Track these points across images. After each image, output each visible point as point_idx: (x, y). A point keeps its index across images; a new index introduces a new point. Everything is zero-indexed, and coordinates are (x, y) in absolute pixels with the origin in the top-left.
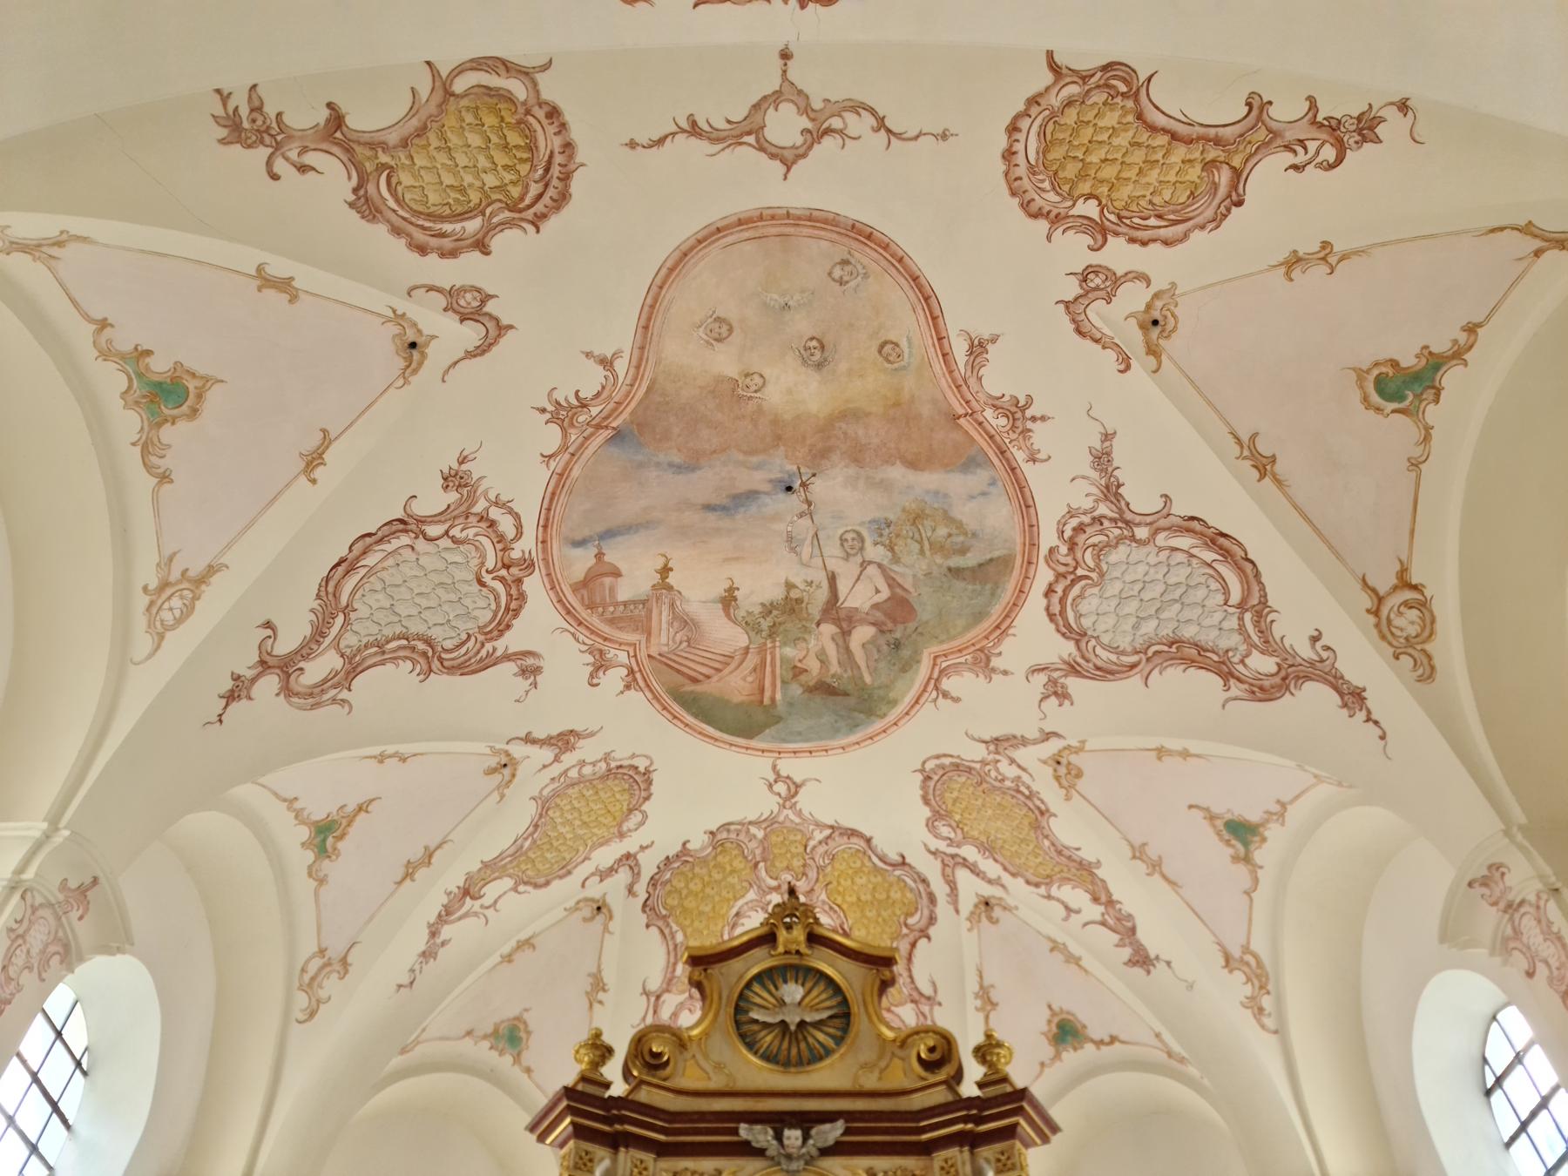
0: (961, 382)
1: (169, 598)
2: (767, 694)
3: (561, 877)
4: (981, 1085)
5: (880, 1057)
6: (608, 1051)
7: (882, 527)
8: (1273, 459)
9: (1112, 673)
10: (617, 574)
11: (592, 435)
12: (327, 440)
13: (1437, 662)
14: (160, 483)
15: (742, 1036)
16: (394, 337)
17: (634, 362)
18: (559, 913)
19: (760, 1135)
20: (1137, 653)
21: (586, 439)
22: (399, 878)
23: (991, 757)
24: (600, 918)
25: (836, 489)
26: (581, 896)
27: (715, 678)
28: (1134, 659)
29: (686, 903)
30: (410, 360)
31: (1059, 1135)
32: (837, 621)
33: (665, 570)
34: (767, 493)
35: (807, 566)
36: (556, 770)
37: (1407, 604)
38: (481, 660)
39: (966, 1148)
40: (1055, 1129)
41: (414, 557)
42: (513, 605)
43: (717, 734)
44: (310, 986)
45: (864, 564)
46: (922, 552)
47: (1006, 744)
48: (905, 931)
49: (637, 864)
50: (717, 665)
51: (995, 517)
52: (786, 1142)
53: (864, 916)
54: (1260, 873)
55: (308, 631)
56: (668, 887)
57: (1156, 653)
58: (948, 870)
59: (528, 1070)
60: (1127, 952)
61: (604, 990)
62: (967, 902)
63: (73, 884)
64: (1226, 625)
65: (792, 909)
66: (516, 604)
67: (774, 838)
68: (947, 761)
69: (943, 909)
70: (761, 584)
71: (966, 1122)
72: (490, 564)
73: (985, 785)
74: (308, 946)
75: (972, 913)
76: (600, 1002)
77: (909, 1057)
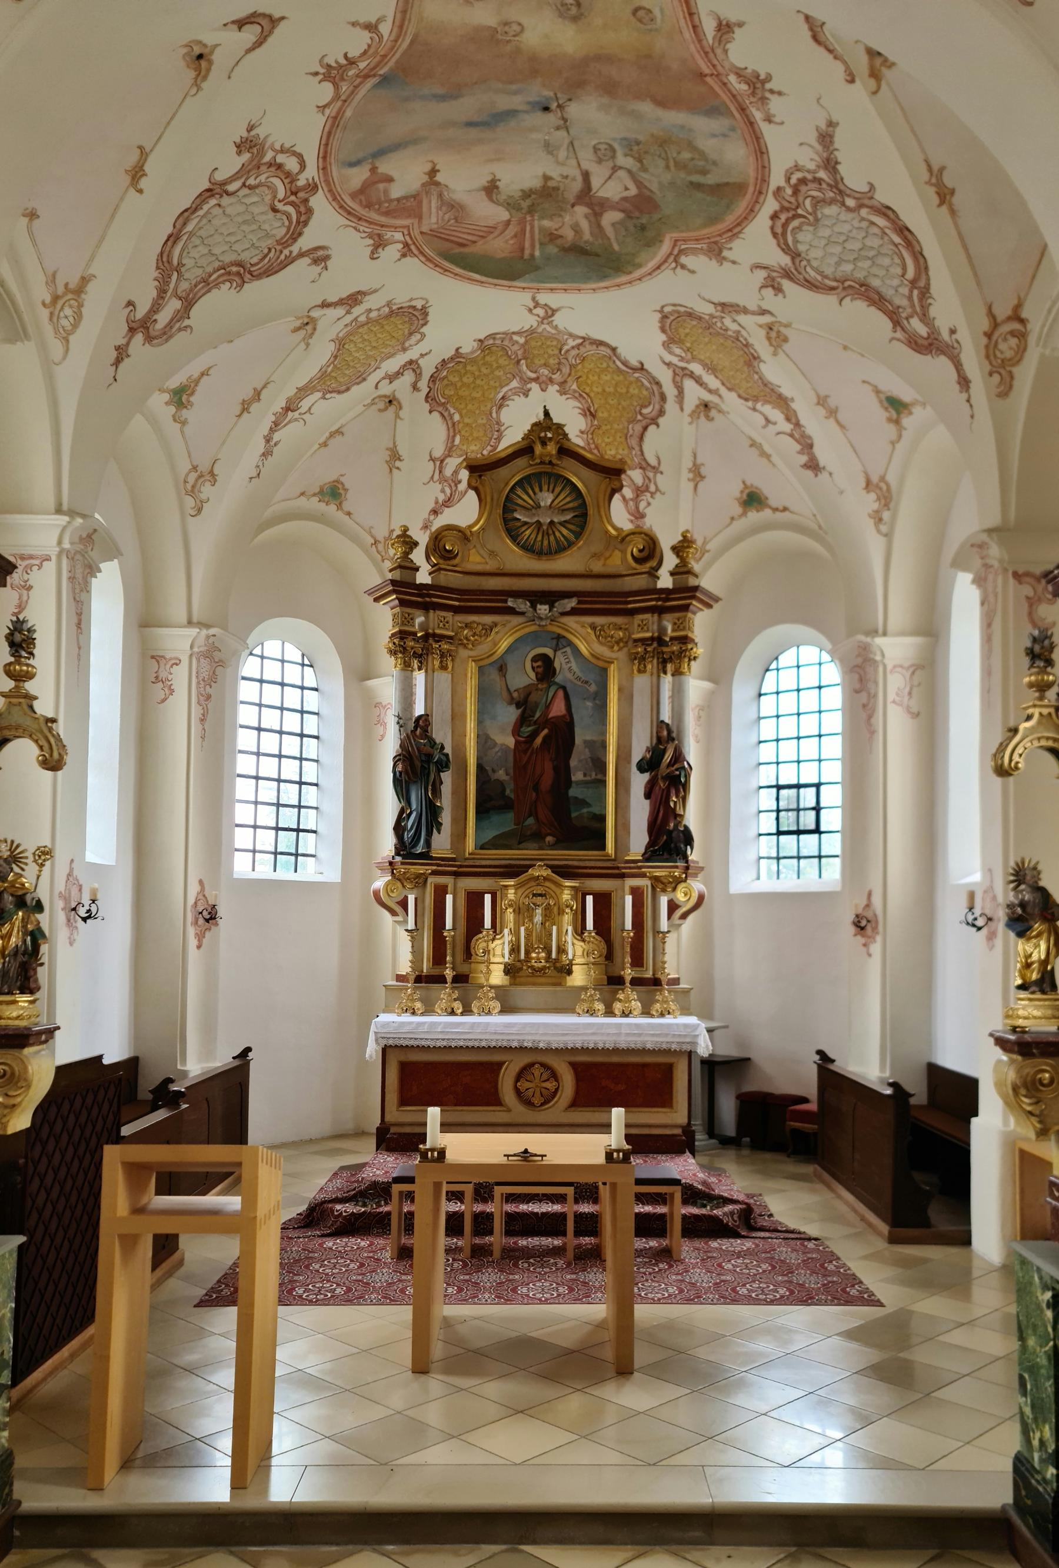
0: (708, 49)
1: (62, 309)
2: (527, 252)
3: (358, 384)
4: (672, 574)
7: (631, 146)
8: (952, 192)
9: (817, 287)
10: (390, 180)
11: (360, 83)
12: (144, 154)
13: (1015, 383)
14: (31, 220)
16: (184, 56)
17: (397, 23)
18: (360, 408)
19: (522, 605)
20: (836, 280)
21: (356, 87)
22: (238, 413)
23: (718, 314)
24: (392, 409)
25: (588, 112)
27: (481, 243)
28: (834, 284)
29: (461, 393)
30: (198, 70)
32: (590, 205)
33: (433, 172)
34: (526, 112)
35: (563, 164)
36: (349, 318)
37: (1013, 333)
38: (282, 262)
39: (656, 615)
40: (717, 600)
41: (220, 211)
42: (303, 218)
43: (484, 279)
44: (193, 492)
45: (615, 169)
46: (667, 167)
47: (731, 309)
48: (639, 417)
49: (419, 367)
50: (481, 234)
51: (734, 155)
54: (904, 433)
55: (154, 294)
56: (445, 382)
57: (850, 287)
58: (678, 379)
60: (804, 459)
63: (84, 536)
64: (901, 290)
66: (305, 215)
67: (533, 343)
68: (682, 309)
69: (671, 406)
70: (521, 174)
72: (281, 194)
73: (711, 330)
74: (184, 466)
75: (694, 412)
76: (398, 468)
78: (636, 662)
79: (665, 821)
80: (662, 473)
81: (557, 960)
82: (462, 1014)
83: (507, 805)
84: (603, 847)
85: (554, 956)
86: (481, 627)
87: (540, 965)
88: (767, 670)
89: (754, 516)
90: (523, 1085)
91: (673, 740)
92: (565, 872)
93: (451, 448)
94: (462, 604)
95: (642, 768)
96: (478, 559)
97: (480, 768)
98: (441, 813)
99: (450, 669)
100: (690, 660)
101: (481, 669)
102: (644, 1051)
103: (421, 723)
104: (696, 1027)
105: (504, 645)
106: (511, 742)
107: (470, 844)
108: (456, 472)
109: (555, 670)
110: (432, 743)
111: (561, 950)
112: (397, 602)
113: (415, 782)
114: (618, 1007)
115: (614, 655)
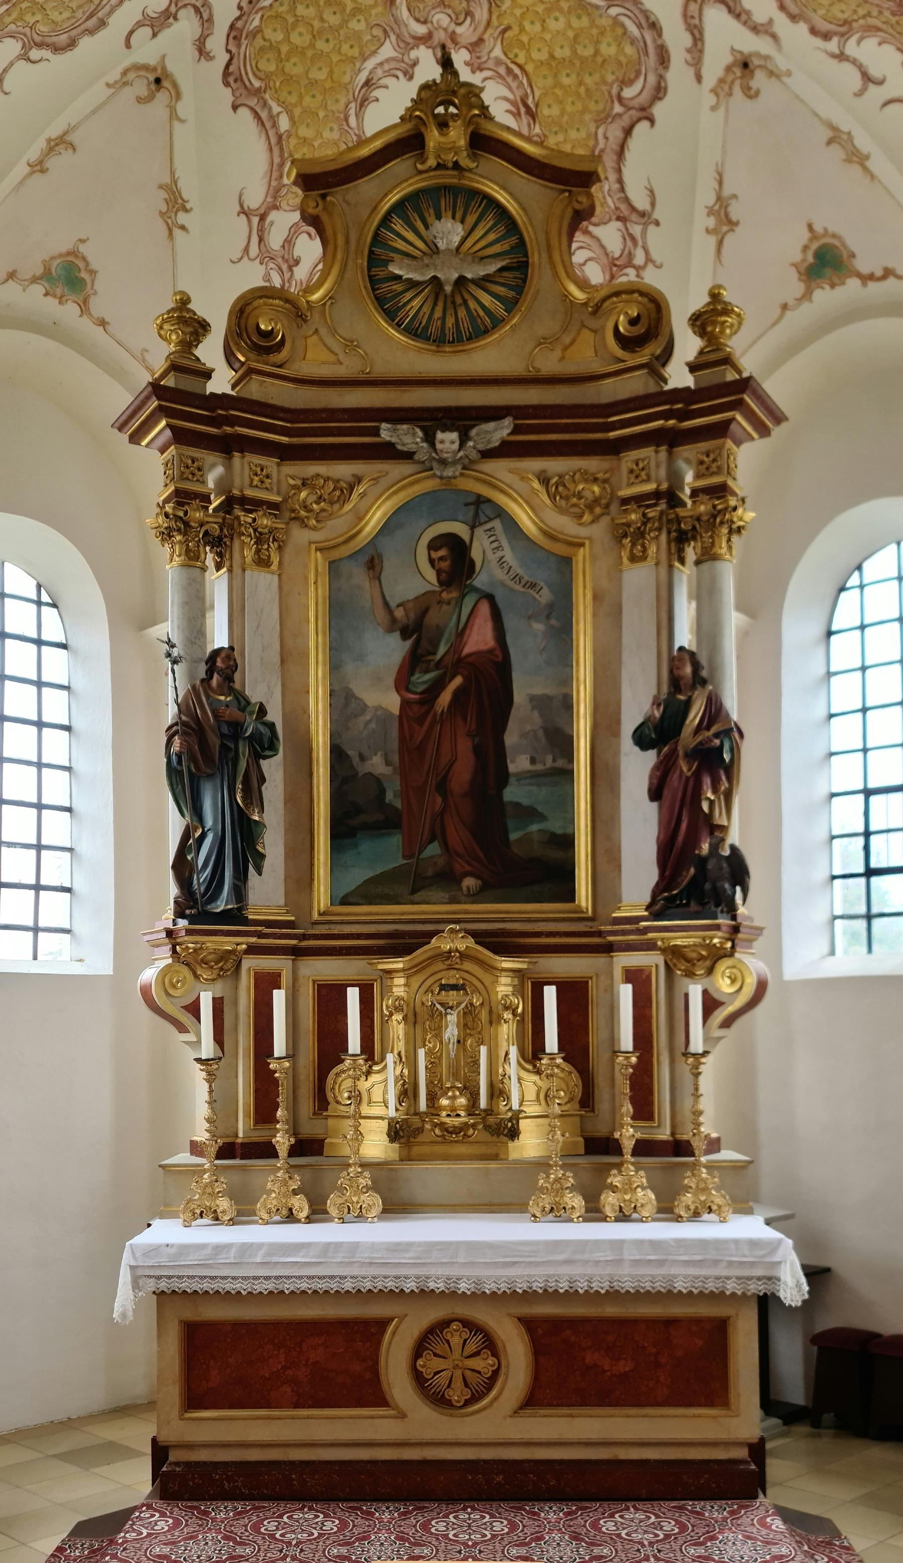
3: (91, 32)
4: (693, 368)
5: (565, 329)
6: (200, 328)
15: (380, 301)
19: (408, 437)
24: (162, 97)
26: (127, 63)
31: (784, 425)
39: (664, 448)
40: (779, 418)
48: (618, 109)
52: (439, 446)
53: (558, 84)
56: (259, 42)
59: (103, 323)
61: (186, 211)
62: (716, 61)
65: (447, 95)
69: (678, 74)
71: (667, 419)
75: (721, 81)
76: (183, 227)
77: (603, 328)
78: (627, 541)
79: (693, 840)
80: (657, 223)
81: (489, 1112)
82: (309, 1220)
83: (389, 822)
84: (570, 895)
85: (483, 1103)
86: (331, 486)
87: (457, 1121)
88: (843, 589)
89: (826, 298)
90: (429, 1364)
91: (704, 682)
92: (501, 943)
93: (277, 190)
94: (295, 440)
95: (642, 739)
96: (325, 355)
97: (337, 753)
98: (260, 835)
99: (274, 567)
100: (731, 532)
101: (334, 567)
102: (670, 1296)
103: (219, 663)
104: (774, 1246)
105: (376, 518)
106: (392, 702)
107: (322, 895)
108: (289, 242)
109: (472, 563)
110: (242, 702)
111: (497, 1092)
112: (168, 433)
113: (210, 776)
114: (609, 1201)
115: (583, 532)
